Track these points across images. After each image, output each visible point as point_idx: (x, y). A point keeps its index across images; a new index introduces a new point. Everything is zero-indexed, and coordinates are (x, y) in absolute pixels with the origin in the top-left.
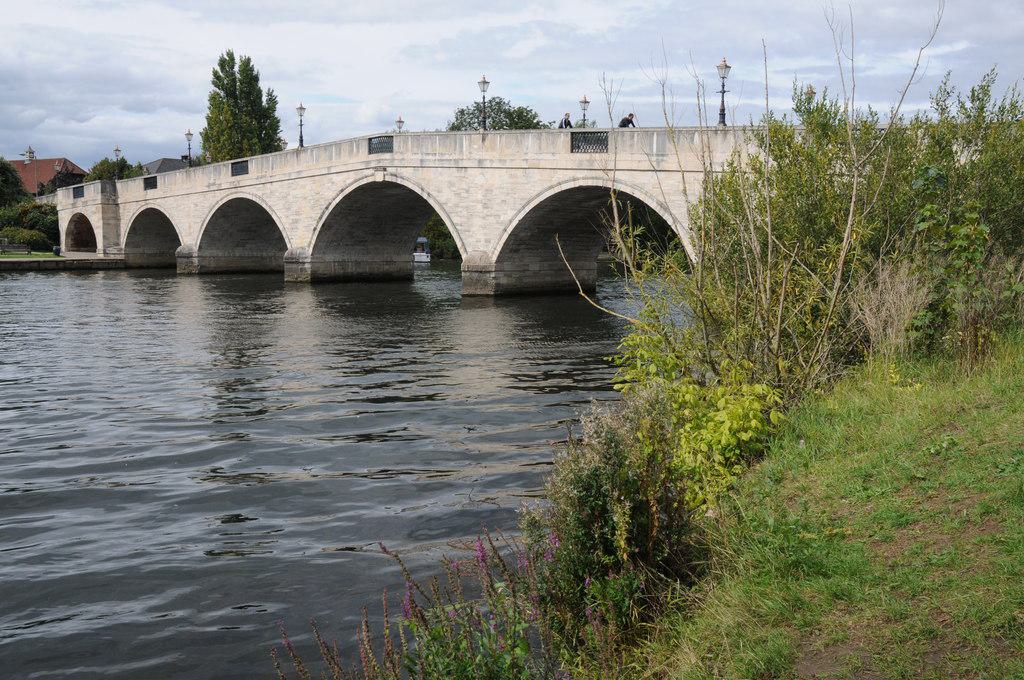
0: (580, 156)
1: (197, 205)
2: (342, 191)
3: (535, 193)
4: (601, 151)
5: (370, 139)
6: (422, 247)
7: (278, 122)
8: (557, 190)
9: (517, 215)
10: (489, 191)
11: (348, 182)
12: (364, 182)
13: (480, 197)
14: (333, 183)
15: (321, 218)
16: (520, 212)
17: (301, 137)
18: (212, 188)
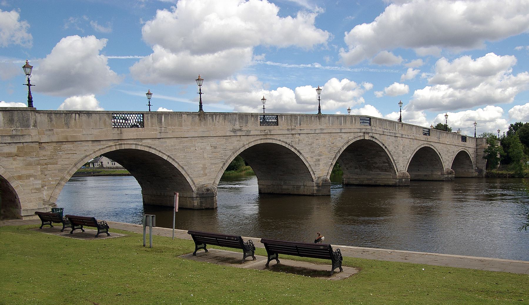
12: (358, 139)
14: (342, 138)
17: (475, 134)
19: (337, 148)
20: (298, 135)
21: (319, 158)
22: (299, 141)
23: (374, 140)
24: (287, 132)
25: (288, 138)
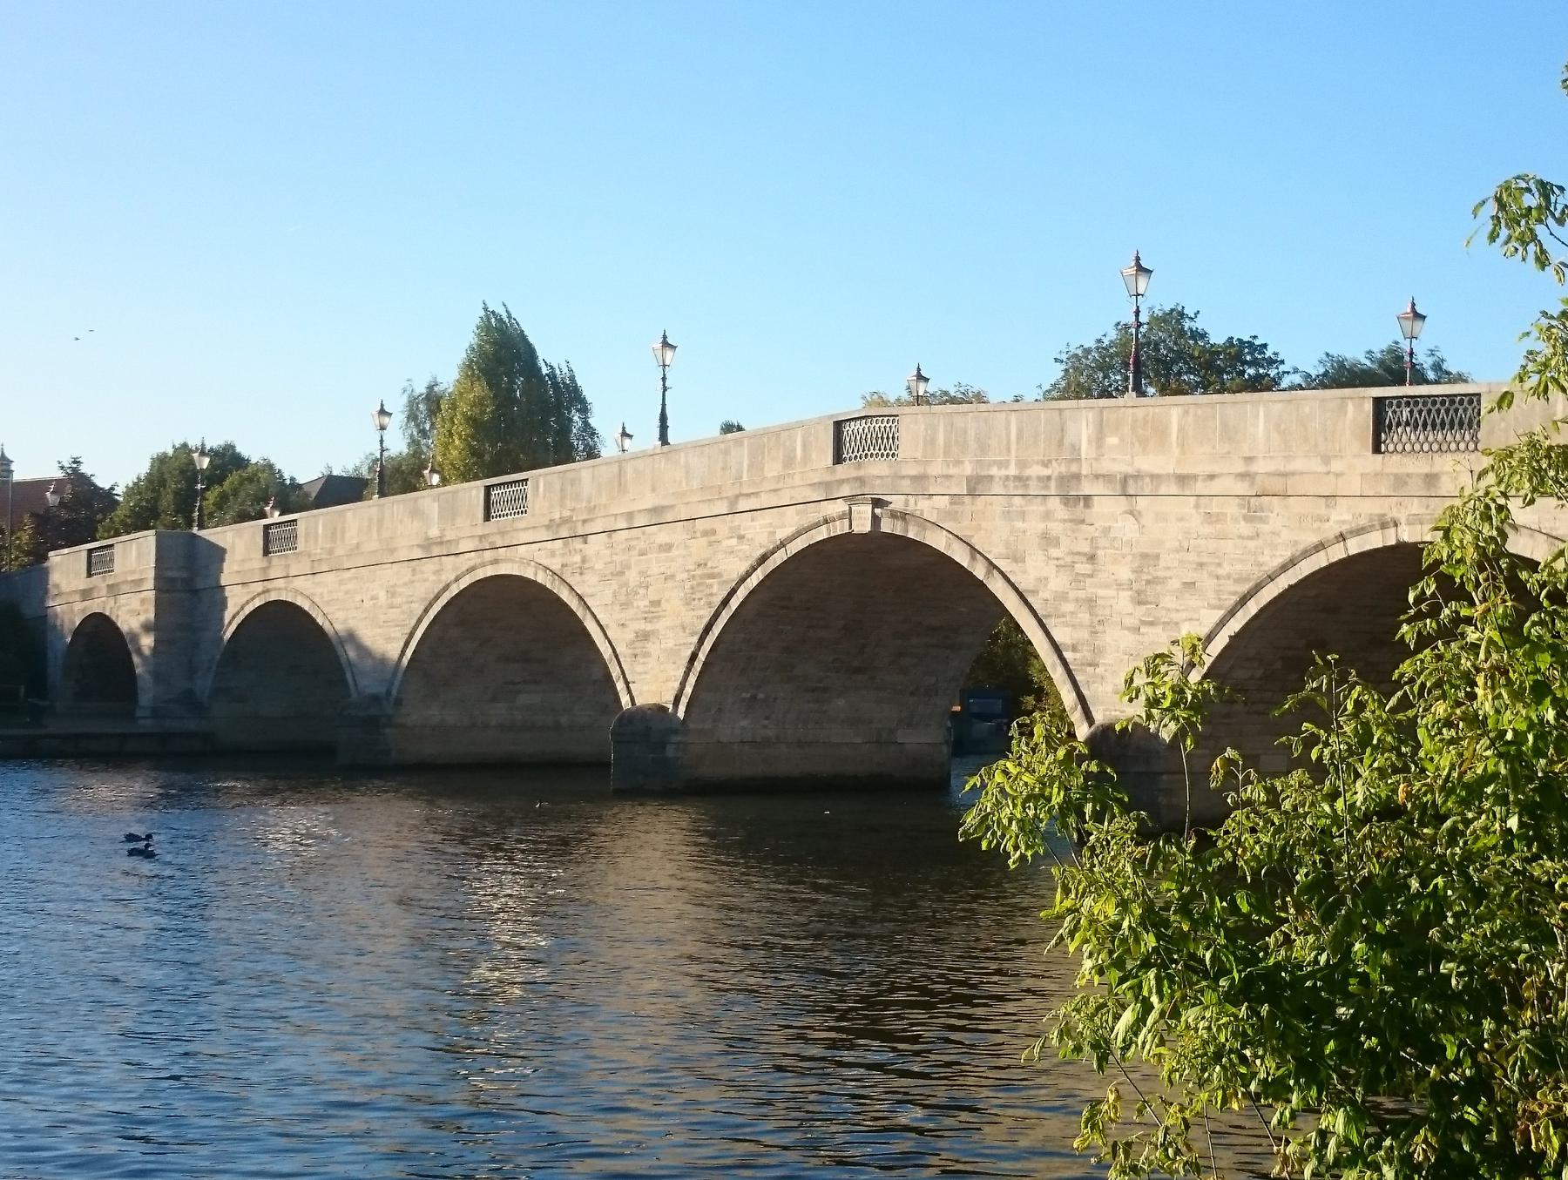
0: (1394, 463)
1: (393, 594)
2: (763, 559)
3: (1277, 562)
4: (228, 557)
5: (838, 426)
6: (1179, 737)
7: (270, 466)
8: (1337, 553)
9: (1222, 623)
10: (1150, 559)
11: (782, 534)
12: (821, 534)
13: (1124, 573)
14: (741, 537)
15: (708, 629)
16: (1232, 613)
17: (663, 418)
18: (436, 551)
19: (719, 583)
20: (579, 540)
21: (649, 627)
22: (584, 561)
23: (911, 535)
24: (544, 535)
25: (553, 554)
